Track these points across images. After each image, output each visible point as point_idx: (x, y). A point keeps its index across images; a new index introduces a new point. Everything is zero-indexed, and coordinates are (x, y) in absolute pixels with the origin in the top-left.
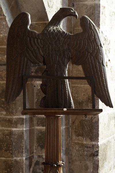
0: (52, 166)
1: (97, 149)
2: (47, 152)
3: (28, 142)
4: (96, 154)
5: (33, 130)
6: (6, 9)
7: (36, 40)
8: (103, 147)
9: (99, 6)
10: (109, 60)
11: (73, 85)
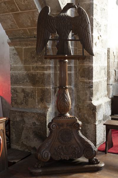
0: (62, 88)
1: (92, 84)
2: (60, 81)
3: (53, 79)
4: (91, 87)
5: (57, 73)
6: (38, 6)
7: (52, 20)
8: (96, 84)
9: (92, 4)
10: (100, 36)
11: (79, 49)
